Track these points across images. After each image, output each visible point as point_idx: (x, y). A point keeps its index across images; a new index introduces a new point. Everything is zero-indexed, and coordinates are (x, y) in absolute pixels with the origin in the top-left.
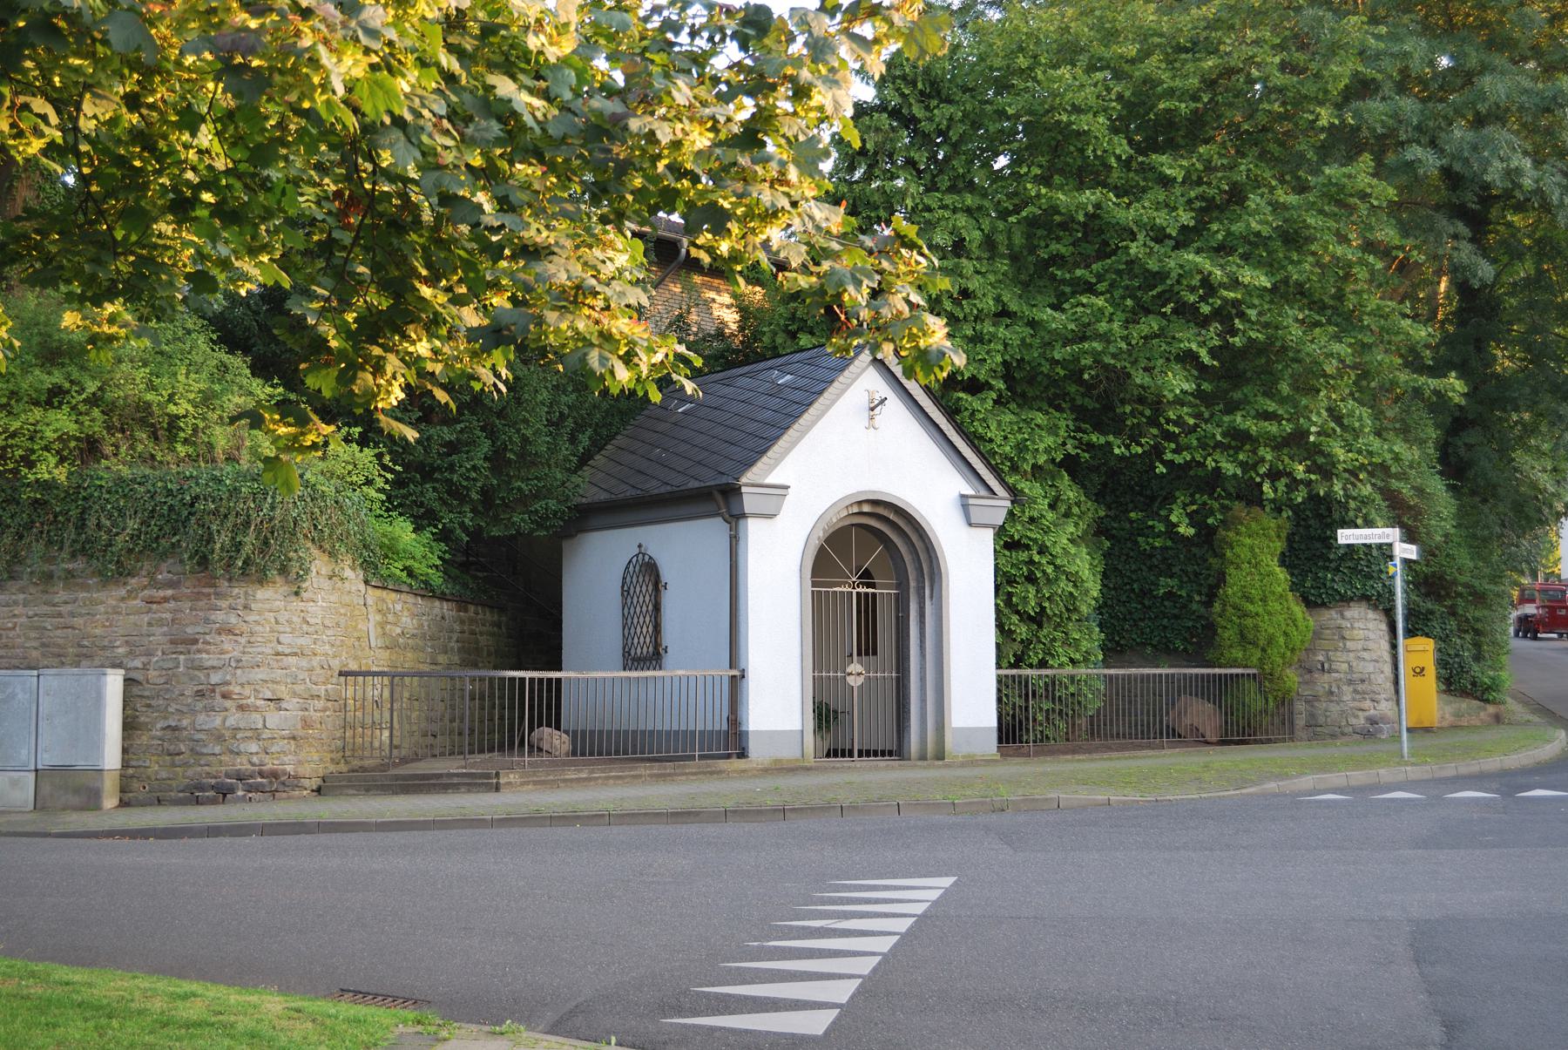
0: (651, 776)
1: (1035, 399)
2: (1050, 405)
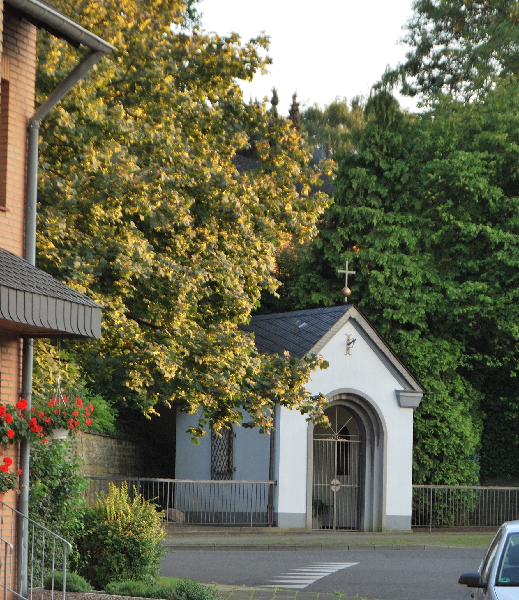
0: (229, 533)
1: (445, 332)
2: (454, 336)
